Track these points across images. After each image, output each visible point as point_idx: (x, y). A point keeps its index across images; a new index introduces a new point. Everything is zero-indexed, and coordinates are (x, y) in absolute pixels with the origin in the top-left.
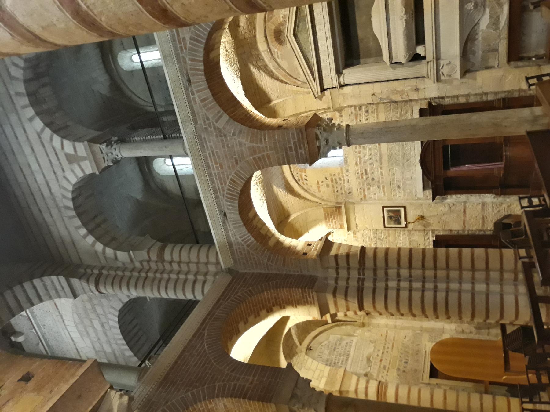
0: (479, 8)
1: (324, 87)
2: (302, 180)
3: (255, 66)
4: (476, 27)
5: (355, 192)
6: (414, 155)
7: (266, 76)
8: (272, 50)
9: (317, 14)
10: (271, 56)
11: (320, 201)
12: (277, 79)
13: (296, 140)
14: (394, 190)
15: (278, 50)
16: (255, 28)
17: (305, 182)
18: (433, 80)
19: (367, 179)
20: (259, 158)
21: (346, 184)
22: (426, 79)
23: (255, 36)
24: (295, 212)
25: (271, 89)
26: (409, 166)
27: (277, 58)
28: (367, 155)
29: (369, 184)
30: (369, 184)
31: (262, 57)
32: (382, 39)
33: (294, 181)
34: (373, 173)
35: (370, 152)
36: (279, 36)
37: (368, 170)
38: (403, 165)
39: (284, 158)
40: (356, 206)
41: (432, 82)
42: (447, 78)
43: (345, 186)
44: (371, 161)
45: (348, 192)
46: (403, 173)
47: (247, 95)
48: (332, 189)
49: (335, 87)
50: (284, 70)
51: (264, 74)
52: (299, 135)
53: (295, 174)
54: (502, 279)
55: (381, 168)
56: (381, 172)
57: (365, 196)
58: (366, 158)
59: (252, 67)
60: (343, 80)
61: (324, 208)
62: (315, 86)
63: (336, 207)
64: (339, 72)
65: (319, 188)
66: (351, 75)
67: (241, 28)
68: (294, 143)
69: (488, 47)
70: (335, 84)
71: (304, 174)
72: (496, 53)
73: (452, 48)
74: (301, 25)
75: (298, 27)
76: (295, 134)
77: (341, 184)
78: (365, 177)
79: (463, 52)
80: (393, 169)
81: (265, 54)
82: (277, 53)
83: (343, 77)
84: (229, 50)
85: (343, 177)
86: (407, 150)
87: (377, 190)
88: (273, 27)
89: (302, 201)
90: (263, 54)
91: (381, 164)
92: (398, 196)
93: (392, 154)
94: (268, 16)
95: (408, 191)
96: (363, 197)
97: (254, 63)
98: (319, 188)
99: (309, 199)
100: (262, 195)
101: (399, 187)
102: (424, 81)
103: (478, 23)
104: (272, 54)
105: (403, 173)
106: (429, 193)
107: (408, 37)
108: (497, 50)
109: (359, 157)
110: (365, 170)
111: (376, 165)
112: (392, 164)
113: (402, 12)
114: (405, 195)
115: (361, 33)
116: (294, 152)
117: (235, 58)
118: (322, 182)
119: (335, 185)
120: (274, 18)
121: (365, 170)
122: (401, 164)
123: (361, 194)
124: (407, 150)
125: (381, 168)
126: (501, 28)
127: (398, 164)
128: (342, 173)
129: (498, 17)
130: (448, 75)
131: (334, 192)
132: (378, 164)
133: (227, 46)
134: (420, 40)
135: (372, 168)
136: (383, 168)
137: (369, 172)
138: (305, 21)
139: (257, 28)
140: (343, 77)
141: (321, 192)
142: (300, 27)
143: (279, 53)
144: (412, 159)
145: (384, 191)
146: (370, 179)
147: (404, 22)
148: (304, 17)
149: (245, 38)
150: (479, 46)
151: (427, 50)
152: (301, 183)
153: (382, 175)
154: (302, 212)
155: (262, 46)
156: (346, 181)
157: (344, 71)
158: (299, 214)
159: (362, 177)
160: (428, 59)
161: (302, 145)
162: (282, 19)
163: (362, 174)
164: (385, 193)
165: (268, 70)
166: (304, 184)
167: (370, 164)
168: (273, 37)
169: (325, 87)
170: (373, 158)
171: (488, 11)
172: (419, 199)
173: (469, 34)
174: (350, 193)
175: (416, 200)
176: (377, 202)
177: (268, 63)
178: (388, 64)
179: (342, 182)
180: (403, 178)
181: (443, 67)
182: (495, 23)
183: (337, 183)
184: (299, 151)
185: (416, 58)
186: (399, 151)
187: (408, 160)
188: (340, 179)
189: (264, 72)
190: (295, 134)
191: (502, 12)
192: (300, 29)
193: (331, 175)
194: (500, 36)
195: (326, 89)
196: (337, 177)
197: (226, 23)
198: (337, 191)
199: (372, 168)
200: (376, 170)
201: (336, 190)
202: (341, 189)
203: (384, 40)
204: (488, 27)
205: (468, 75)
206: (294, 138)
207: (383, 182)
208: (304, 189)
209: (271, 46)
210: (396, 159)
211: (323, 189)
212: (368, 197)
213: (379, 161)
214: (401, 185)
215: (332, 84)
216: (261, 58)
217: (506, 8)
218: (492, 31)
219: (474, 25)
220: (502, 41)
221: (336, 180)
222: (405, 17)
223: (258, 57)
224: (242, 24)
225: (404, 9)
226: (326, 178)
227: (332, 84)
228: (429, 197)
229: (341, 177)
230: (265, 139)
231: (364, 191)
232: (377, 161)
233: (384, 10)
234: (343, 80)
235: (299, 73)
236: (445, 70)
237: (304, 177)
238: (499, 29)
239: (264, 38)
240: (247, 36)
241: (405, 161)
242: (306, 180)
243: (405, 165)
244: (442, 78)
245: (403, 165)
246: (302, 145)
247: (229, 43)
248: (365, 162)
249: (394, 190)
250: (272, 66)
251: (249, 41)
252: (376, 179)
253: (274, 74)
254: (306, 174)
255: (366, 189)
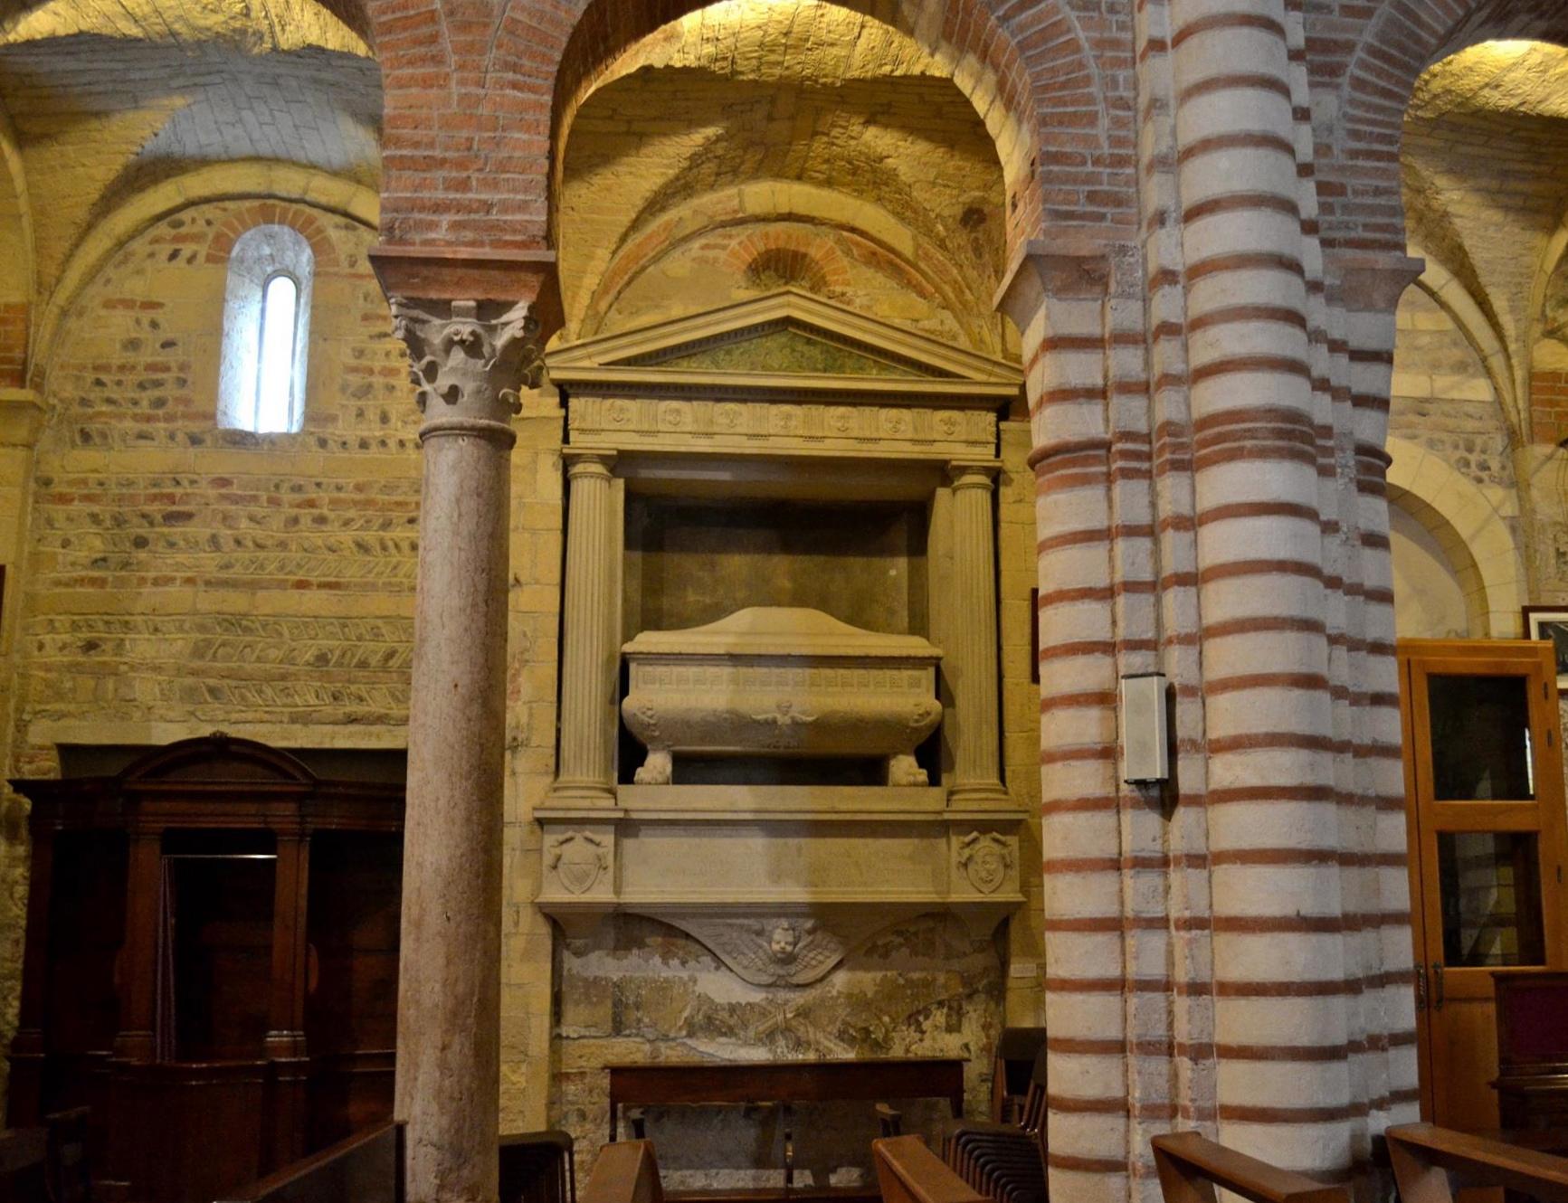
0: (772, 968)
1: (577, 396)
2: (176, 239)
3: (710, 144)
4: (707, 959)
5: (86, 460)
6: (234, 716)
7: (660, 181)
8: (734, 231)
9: (842, 417)
10: (719, 218)
11: (61, 297)
12: (635, 225)
13: (494, 216)
14: (75, 627)
15: (734, 254)
16: (829, 183)
17: (167, 249)
18: (547, 804)
19: (144, 516)
20: (433, 39)
21: (129, 425)
22: (551, 778)
23: (799, 178)
24: (27, 172)
25: (609, 189)
26: (190, 694)
27: (703, 241)
28: (259, 533)
29: (119, 521)
30: (119, 521)
31: (723, 186)
32: (706, 633)
33: (179, 200)
34: (172, 545)
35: (269, 543)
36: (780, 266)
37: (190, 529)
38: (193, 673)
39: (416, 145)
40: (21, 453)
41: (536, 802)
42: (548, 859)
43: (121, 417)
44: (228, 544)
45: (93, 427)
46: (158, 669)
47: (647, 70)
48: (116, 361)
49: (566, 440)
50: (656, 259)
51: (672, 173)
52: (515, 231)
53: (209, 211)
54: (1198, 861)
55: (190, 581)
56: (171, 580)
57: (63, 499)
58: (244, 524)
59: (711, 131)
60: (592, 475)
61: (25, 309)
62: (586, 363)
63: (25, 363)
64: (620, 463)
65: (128, 304)
66: (600, 503)
67: (856, 129)
68: (487, 207)
69: (632, 999)
70: (578, 442)
71: (203, 250)
72: (608, 1026)
73: (657, 877)
74: (815, 352)
75: (809, 342)
76: (518, 217)
77: (135, 403)
78: (155, 509)
79: (626, 915)
80: (181, 629)
81: (730, 198)
82: (724, 248)
83: (599, 476)
84: (817, 54)
85: (170, 418)
86: (260, 692)
87: (82, 555)
88: (815, 252)
89: (82, 214)
90: (732, 191)
91: (208, 583)
92: (47, 638)
93: (247, 630)
94: (857, 244)
95: (68, 685)
96: (57, 489)
97: (720, 149)
98: (128, 304)
99: (81, 252)
100: (177, 27)
101: (91, 646)
102: (547, 773)
103: (720, 963)
104: (723, 225)
105: (158, 669)
106: (48, 767)
107: (712, 727)
108: (618, 1028)
109: (255, 498)
110: (188, 516)
111: (209, 562)
112: (202, 628)
113: (803, 713)
114: (48, 668)
115: (736, 564)
116: (440, 195)
117: (777, 71)
118: (154, 325)
119: (130, 379)
120: (845, 262)
121: (188, 516)
122: (196, 664)
123: (71, 483)
124: (260, 692)
125: (190, 581)
126: (689, 1042)
127: (198, 653)
128: (185, 416)
129: (730, 1032)
130: (559, 858)
131: (105, 368)
132: (212, 571)
133: (834, 51)
134: (689, 768)
135: (193, 545)
136: (188, 590)
137: (177, 531)
138: (825, 371)
139: (825, 194)
140: (599, 476)
141: (103, 312)
142: (806, 349)
143: (722, 255)
144: (216, 709)
145: (81, 581)
146: (144, 531)
147: (770, 716)
148: (841, 369)
149: (815, 133)
150: (643, 967)
151: (655, 785)
152: (163, 229)
153: (156, 582)
154: (23, 205)
155: (762, 194)
156: (145, 427)
157: (620, 484)
158: (20, 184)
159: (154, 498)
160: (623, 790)
161: (469, 235)
162: (838, 289)
163: (171, 498)
164: (67, 585)
165: (674, 194)
166: (156, 241)
167: (214, 540)
168: (781, 244)
169: (573, 402)
170: (239, 554)
171: (758, 997)
172: (22, 727)
173: (688, 936)
174: (86, 437)
175: (20, 710)
176: (27, 549)
177: (695, 202)
178: (628, 648)
179: (145, 408)
180: (133, 668)
181: (591, 841)
182: (713, 1022)
183: (142, 386)
184: (446, 219)
185: (629, 753)
186: (259, 659)
187: (212, 691)
188: (160, 403)
189: (677, 178)
190: (518, 217)
191: (746, 1044)
192: (800, 347)
193: (183, 367)
194: (666, 1038)
195: (564, 404)
196: (170, 391)
197: (956, 61)
198: (99, 383)
199: (193, 545)
200: (180, 558)
201: (104, 377)
202: (110, 401)
203: (716, 639)
204: (703, 999)
205: (544, 930)
206: (506, 207)
207: (121, 583)
208: (132, 237)
209: (750, 229)
210: (223, 644)
211: (121, 323)
212: (59, 512)
213: (224, 575)
214: (95, 658)
215: (582, 431)
216: (723, 179)
217: (759, 1055)
218: (685, 1014)
219: (718, 953)
220: (647, 1047)
221: (158, 384)
222: (783, 720)
223: (730, 171)
224: (871, 133)
225: (810, 719)
226: (167, 344)
227: (582, 431)
228: (26, 768)
229: (170, 407)
230: (515, 86)
231: (88, 498)
232: (228, 566)
233: (819, 652)
234: (592, 475)
235: (636, 313)
236: (577, 850)
237: (187, 249)
238: (690, 1035)
239: (784, 210)
240: (819, 145)
241: (211, 682)
242: (174, 255)
243: (189, 681)
244: (550, 838)
245: (193, 673)
246: (469, 235)
247: (836, 67)
248: (226, 519)
249: (75, 627)
250: (682, 213)
251: (799, 146)
252: (142, 555)
253: (653, 214)
254: (201, 258)
255: (96, 509)
